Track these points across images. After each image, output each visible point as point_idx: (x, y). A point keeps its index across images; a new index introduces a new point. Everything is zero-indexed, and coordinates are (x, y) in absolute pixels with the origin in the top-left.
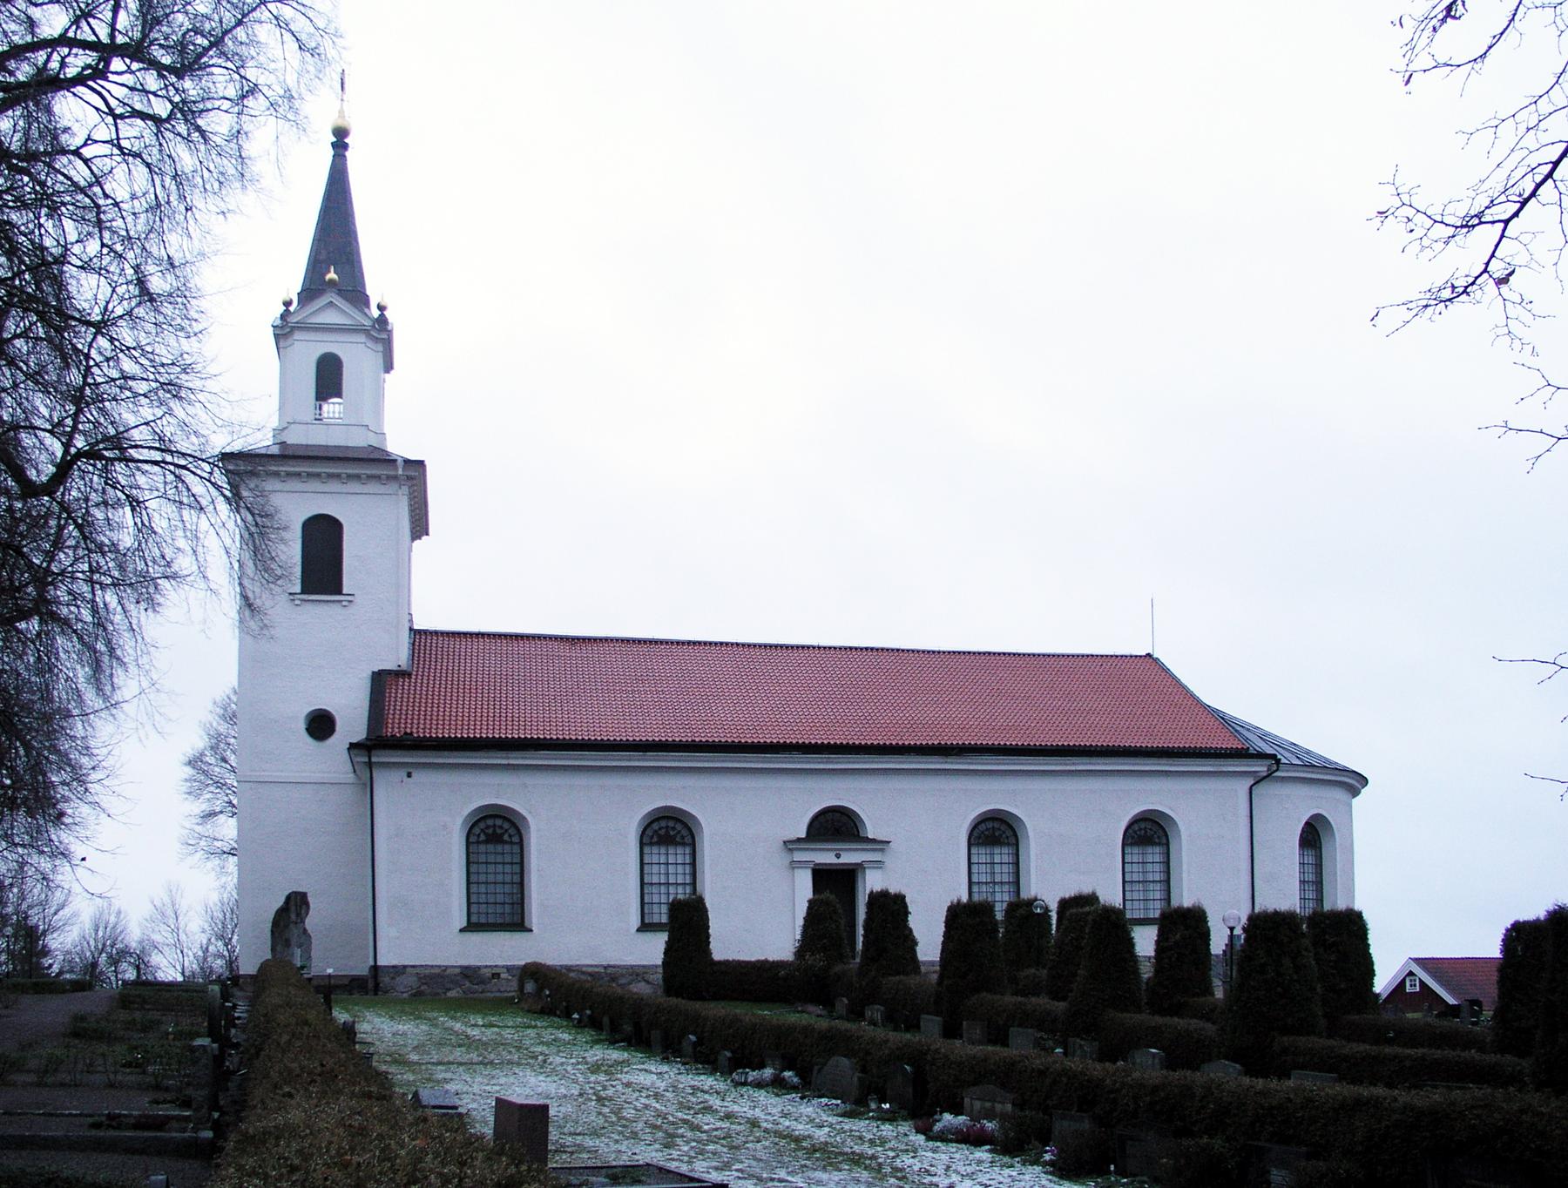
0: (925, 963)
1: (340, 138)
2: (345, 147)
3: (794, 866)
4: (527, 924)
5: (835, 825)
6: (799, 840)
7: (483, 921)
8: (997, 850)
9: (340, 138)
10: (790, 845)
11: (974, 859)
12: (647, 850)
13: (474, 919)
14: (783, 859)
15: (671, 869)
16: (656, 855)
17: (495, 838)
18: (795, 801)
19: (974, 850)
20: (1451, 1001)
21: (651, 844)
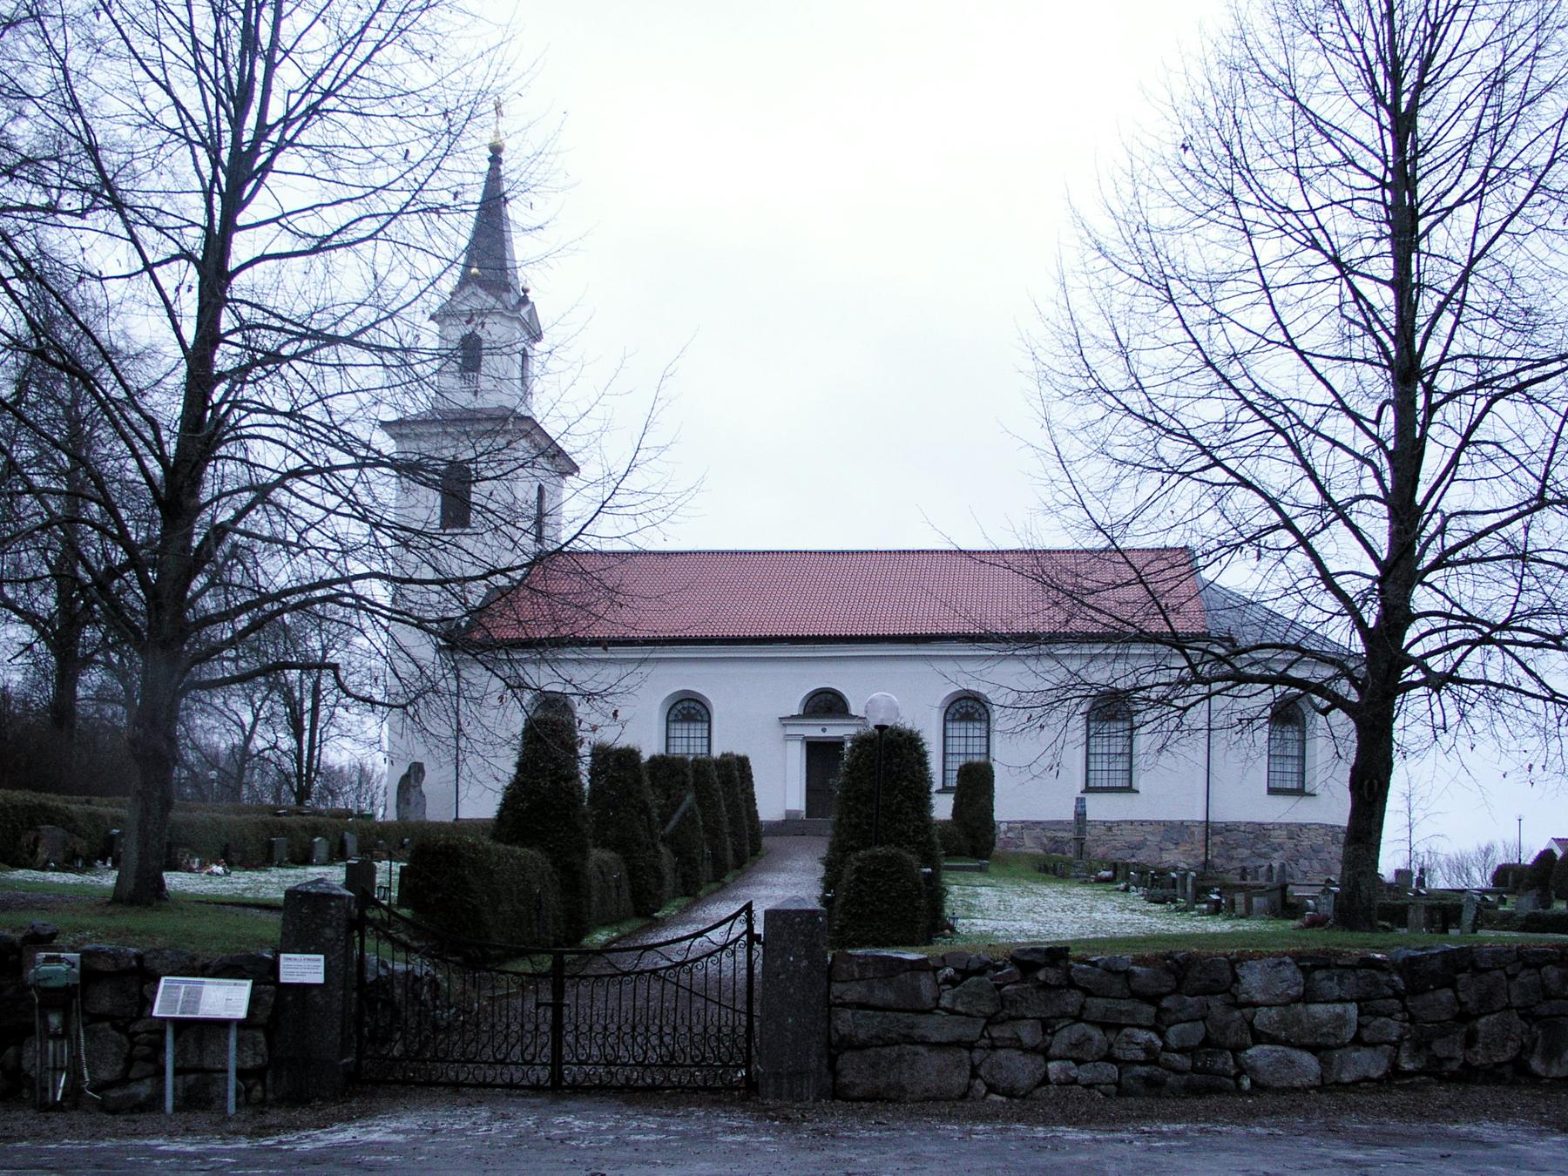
0: (1094, 824)
1: (496, 153)
2: (500, 161)
3: (788, 738)
4: (1134, 787)
5: (827, 704)
6: (798, 717)
7: (1105, 784)
8: (692, 726)
9: (496, 153)
10: (785, 721)
11: (950, 733)
12: (672, 726)
13: (1091, 784)
14: (779, 732)
15: (685, 741)
16: (956, 729)
17: (967, 717)
18: (792, 683)
19: (949, 725)
20: (175, 881)
21: (953, 720)
